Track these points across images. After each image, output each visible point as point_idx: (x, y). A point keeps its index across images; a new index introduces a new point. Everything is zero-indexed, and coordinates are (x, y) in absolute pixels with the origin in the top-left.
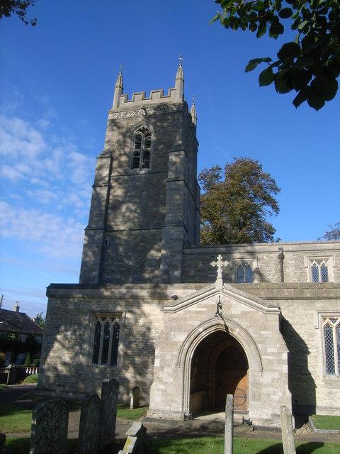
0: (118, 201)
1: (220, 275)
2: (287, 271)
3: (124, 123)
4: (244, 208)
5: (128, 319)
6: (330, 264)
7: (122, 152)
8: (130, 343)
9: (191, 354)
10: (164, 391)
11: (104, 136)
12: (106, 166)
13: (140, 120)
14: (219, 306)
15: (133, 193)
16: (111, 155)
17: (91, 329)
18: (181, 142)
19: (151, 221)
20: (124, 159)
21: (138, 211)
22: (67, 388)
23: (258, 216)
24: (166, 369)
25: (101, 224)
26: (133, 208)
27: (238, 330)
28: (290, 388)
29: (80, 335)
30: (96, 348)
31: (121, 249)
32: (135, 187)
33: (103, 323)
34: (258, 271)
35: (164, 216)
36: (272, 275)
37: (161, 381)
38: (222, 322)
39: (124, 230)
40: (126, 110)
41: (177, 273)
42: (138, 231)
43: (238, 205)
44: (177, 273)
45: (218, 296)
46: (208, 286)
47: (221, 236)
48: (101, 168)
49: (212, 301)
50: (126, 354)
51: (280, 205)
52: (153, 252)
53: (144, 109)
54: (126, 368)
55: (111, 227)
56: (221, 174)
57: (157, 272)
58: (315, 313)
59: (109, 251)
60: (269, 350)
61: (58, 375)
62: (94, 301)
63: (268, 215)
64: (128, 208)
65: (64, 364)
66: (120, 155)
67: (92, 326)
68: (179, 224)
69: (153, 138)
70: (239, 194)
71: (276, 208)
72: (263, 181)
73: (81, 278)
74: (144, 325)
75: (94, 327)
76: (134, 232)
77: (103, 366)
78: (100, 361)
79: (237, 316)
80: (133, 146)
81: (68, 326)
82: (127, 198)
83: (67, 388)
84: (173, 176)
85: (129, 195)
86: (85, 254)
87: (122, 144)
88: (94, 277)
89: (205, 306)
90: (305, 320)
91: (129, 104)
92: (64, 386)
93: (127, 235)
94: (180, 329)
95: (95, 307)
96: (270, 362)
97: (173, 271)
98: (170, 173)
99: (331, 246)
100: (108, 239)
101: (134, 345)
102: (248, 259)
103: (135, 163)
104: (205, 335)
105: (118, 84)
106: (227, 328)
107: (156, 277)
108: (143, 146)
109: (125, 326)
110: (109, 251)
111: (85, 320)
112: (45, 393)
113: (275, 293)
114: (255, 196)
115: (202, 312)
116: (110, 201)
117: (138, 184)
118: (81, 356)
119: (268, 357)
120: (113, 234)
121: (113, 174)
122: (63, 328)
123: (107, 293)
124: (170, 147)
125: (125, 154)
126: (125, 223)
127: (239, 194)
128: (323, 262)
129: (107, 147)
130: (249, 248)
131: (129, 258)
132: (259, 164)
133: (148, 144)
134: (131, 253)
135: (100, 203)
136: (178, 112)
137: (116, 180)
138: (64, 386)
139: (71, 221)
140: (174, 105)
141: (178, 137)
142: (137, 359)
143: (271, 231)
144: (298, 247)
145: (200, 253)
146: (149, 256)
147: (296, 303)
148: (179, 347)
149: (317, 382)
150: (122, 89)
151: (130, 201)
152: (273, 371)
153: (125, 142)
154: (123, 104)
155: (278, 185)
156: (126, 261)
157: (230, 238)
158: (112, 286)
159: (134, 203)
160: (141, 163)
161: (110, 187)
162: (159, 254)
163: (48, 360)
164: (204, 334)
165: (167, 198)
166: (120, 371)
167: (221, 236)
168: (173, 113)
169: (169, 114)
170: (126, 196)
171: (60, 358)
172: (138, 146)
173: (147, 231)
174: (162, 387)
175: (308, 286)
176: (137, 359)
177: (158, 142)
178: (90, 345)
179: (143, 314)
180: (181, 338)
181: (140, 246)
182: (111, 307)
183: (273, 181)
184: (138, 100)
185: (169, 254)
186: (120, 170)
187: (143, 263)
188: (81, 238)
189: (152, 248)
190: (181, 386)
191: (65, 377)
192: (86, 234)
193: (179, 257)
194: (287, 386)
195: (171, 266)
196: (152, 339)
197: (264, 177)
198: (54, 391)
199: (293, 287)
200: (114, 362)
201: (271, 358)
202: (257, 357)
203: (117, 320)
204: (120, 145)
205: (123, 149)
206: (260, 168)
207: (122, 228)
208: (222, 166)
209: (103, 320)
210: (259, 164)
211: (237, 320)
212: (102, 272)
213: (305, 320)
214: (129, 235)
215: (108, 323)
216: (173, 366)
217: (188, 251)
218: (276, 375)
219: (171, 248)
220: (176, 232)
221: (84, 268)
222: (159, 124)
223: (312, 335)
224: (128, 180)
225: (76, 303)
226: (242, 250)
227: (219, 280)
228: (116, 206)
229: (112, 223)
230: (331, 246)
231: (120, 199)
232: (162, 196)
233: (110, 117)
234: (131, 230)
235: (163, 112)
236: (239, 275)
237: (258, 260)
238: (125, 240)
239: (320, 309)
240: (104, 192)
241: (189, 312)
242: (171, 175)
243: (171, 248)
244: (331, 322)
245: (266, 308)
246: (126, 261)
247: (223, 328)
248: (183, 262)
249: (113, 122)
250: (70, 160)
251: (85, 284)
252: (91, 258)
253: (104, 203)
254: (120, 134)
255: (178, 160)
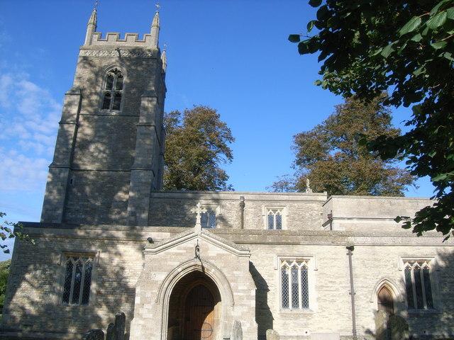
0: (87, 140)
1: (198, 221)
2: (246, 218)
3: (96, 61)
4: (200, 155)
5: (101, 259)
6: (284, 213)
7: (93, 91)
8: (103, 282)
9: (169, 292)
10: (144, 326)
11: (75, 72)
12: (76, 103)
13: (114, 61)
14: (197, 248)
15: (103, 134)
16: (81, 93)
17: (63, 268)
18: (153, 88)
19: (119, 163)
20: (94, 98)
21: (107, 152)
22: (35, 327)
23: (212, 162)
24: (146, 306)
25: (67, 162)
26: (102, 149)
27: (213, 270)
28: (257, 320)
29: (51, 275)
30: (67, 286)
31: (88, 189)
32: (104, 128)
33: (74, 263)
34: (222, 218)
35: (133, 158)
36: (233, 218)
37: (140, 316)
38: (199, 263)
39: (91, 170)
40: (99, 49)
41: (144, 216)
42: (106, 172)
43: (194, 152)
44: (144, 216)
45: (196, 239)
46: (189, 230)
47: (178, 180)
48: (70, 104)
49: (191, 244)
50: (99, 293)
51: (234, 154)
52: (120, 194)
53: (119, 51)
54: (99, 305)
55: (77, 166)
56: (179, 119)
57: (123, 213)
58: (275, 256)
59: (75, 190)
60: (240, 288)
61: (25, 315)
62: (67, 241)
63: (222, 162)
64: (96, 148)
65: (32, 303)
66: (91, 94)
67: (64, 265)
68: (147, 168)
69: (125, 79)
70: (197, 141)
71: (229, 156)
72: (220, 130)
73: (43, 216)
74: (117, 265)
75: (65, 266)
76: (102, 173)
77: (74, 305)
78: (70, 300)
79: (213, 258)
80: (105, 85)
81: (38, 265)
82: (97, 137)
83: (35, 327)
84: (145, 121)
85: (98, 134)
86: (49, 191)
87: (93, 83)
88: (57, 216)
89: (185, 249)
90: (267, 262)
91: (102, 43)
92: (31, 326)
93: (94, 175)
94: (160, 269)
95: (68, 247)
96: (241, 298)
97: (140, 213)
98: (141, 118)
99: (286, 197)
100: (74, 177)
101: (107, 284)
102: (213, 205)
103: (105, 103)
104: (183, 274)
105: (91, 20)
106: (203, 268)
107: (123, 218)
108: (114, 88)
109: (98, 266)
110: (75, 190)
111: (57, 260)
112: (10, 334)
113: (242, 239)
114: (211, 143)
115: (181, 254)
116: (78, 139)
117: (108, 125)
118: (51, 295)
119: (239, 294)
120: (80, 172)
121: (81, 112)
122: (32, 267)
123: (81, 233)
124: (143, 92)
125: (96, 93)
126: (93, 162)
127: (197, 141)
128: (279, 211)
129: (77, 84)
130: (215, 196)
131: (95, 198)
132: (217, 113)
133: (120, 86)
134: (97, 194)
135: (67, 140)
136: (152, 58)
137: (86, 118)
138: (31, 326)
139: (13, 152)
140: (149, 51)
141: (151, 83)
142: (111, 298)
143: (224, 177)
144: (258, 197)
145: (167, 198)
146: (116, 198)
147: (260, 247)
148: (158, 286)
149: (274, 315)
150: (96, 26)
151: (98, 141)
152: (242, 305)
153: (97, 81)
154: (95, 42)
155: (233, 135)
156: (93, 202)
157: (186, 182)
158: (86, 226)
159: (103, 144)
160: (112, 105)
161: (78, 125)
162: (127, 197)
163: (14, 300)
164: (182, 274)
165: (137, 142)
166: (92, 310)
167: (178, 180)
168: (148, 59)
169: (144, 59)
170: (95, 136)
171: (28, 298)
172: (110, 86)
173: (114, 173)
174: (142, 322)
175: (266, 233)
176: (111, 298)
177: (131, 85)
178: (61, 284)
179: (118, 254)
180: (160, 277)
181: (107, 187)
182: (84, 247)
183: (229, 131)
184: (112, 41)
185: (137, 196)
186: (90, 109)
187: (108, 207)
188: (46, 176)
189: (120, 190)
190: (160, 321)
191: (32, 317)
192: (50, 171)
193: (146, 200)
194: (254, 318)
195: (139, 208)
196: (125, 278)
197: (221, 125)
198: (21, 331)
199: (251, 232)
200: (86, 300)
201: (242, 294)
202: (229, 293)
203: (90, 259)
204: (92, 84)
205: (95, 88)
206: (217, 117)
207: (89, 168)
208: (182, 111)
209: (75, 260)
210: (217, 113)
211: (212, 261)
212: (66, 210)
213: (267, 262)
214: (97, 175)
215: (80, 262)
216: (153, 303)
217: (156, 195)
218: (245, 309)
219: (375, 260)
220: (145, 176)
221: (48, 206)
222: (133, 67)
223: (271, 275)
224: (97, 119)
225: (46, 242)
226: (208, 197)
227: (198, 226)
228: (84, 145)
229: (80, 162)
230: (286, 197)
231: (88, 138)
232: (131, 139)
233: (82, 53)
234: (99, 170)
235: (137, 57)
236: (209, 220)
237: (223, 207)
238: (92, 180)
239: (279, 252)
240: (72, 129)
241: (169, 253)
242: (143, 120)
243: (375, 260)
244: (287, 264)
245: (238, 251)
246: (93, 202)
247: (200, 269)
248: (151, 204)
249: (85, 58)
250: (20, 88)
251: (49, 221)
252: (55, 196)
253: (71, 141)
254: (92, 72)
255: (150, 105)
